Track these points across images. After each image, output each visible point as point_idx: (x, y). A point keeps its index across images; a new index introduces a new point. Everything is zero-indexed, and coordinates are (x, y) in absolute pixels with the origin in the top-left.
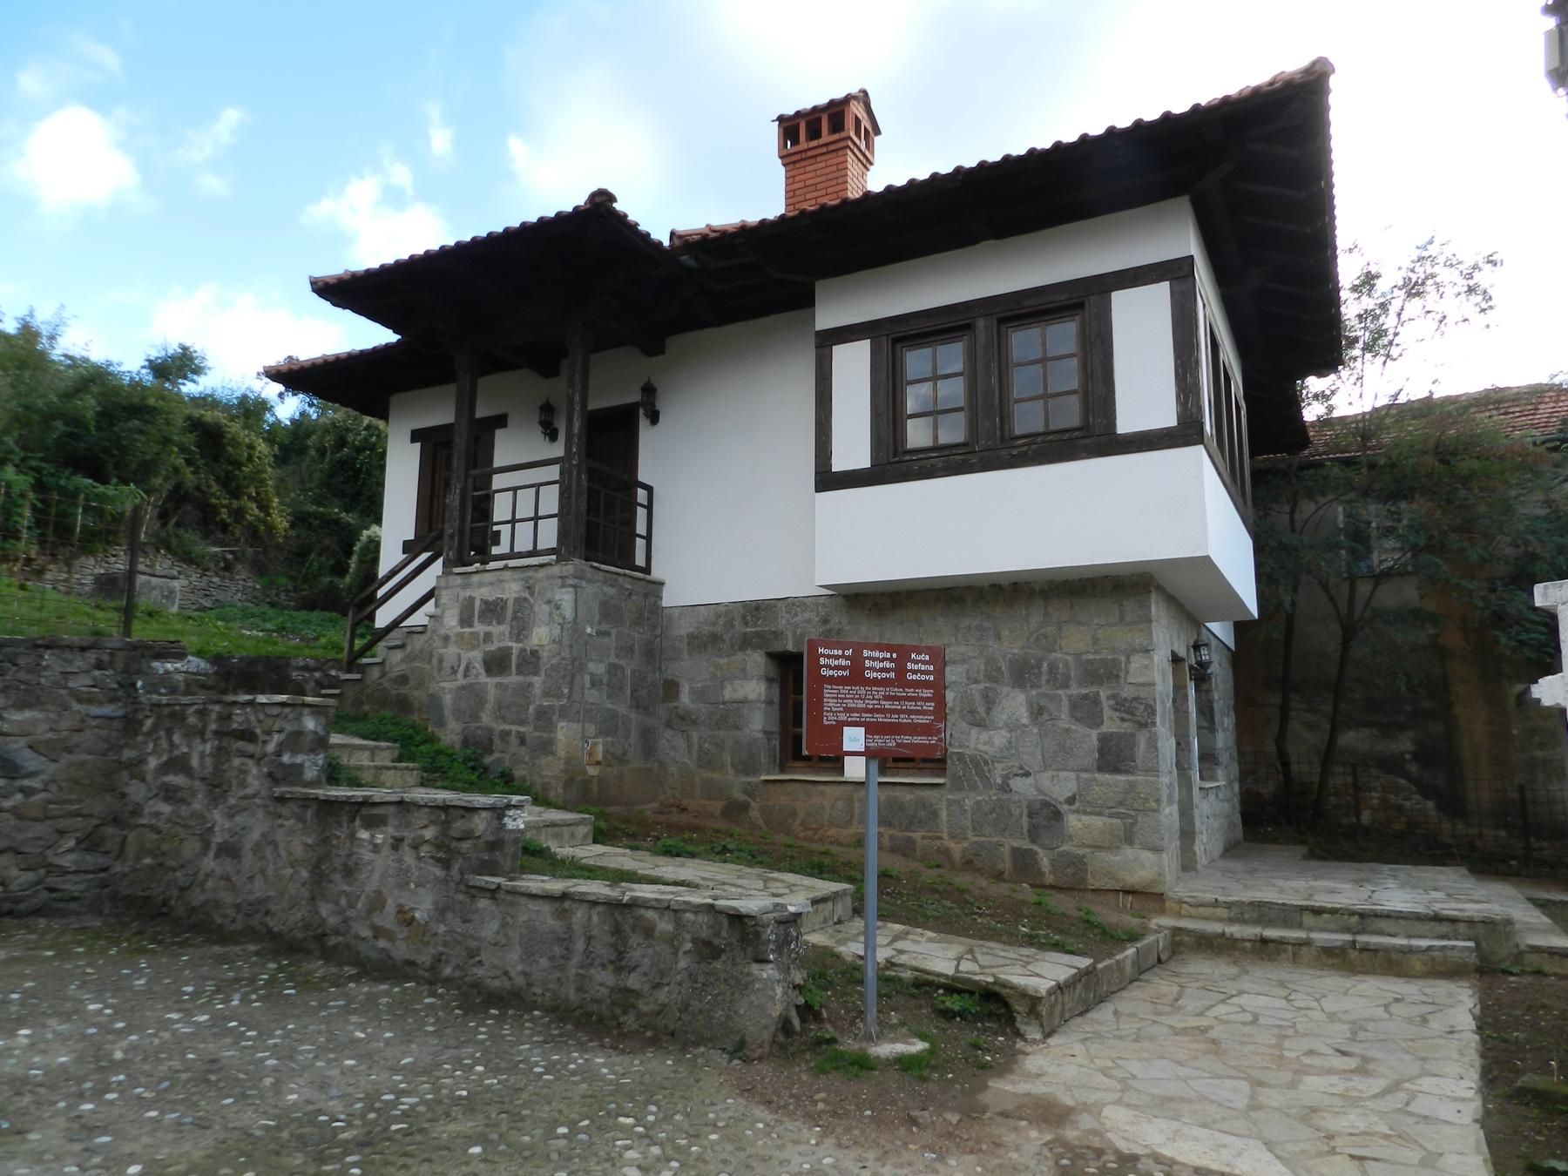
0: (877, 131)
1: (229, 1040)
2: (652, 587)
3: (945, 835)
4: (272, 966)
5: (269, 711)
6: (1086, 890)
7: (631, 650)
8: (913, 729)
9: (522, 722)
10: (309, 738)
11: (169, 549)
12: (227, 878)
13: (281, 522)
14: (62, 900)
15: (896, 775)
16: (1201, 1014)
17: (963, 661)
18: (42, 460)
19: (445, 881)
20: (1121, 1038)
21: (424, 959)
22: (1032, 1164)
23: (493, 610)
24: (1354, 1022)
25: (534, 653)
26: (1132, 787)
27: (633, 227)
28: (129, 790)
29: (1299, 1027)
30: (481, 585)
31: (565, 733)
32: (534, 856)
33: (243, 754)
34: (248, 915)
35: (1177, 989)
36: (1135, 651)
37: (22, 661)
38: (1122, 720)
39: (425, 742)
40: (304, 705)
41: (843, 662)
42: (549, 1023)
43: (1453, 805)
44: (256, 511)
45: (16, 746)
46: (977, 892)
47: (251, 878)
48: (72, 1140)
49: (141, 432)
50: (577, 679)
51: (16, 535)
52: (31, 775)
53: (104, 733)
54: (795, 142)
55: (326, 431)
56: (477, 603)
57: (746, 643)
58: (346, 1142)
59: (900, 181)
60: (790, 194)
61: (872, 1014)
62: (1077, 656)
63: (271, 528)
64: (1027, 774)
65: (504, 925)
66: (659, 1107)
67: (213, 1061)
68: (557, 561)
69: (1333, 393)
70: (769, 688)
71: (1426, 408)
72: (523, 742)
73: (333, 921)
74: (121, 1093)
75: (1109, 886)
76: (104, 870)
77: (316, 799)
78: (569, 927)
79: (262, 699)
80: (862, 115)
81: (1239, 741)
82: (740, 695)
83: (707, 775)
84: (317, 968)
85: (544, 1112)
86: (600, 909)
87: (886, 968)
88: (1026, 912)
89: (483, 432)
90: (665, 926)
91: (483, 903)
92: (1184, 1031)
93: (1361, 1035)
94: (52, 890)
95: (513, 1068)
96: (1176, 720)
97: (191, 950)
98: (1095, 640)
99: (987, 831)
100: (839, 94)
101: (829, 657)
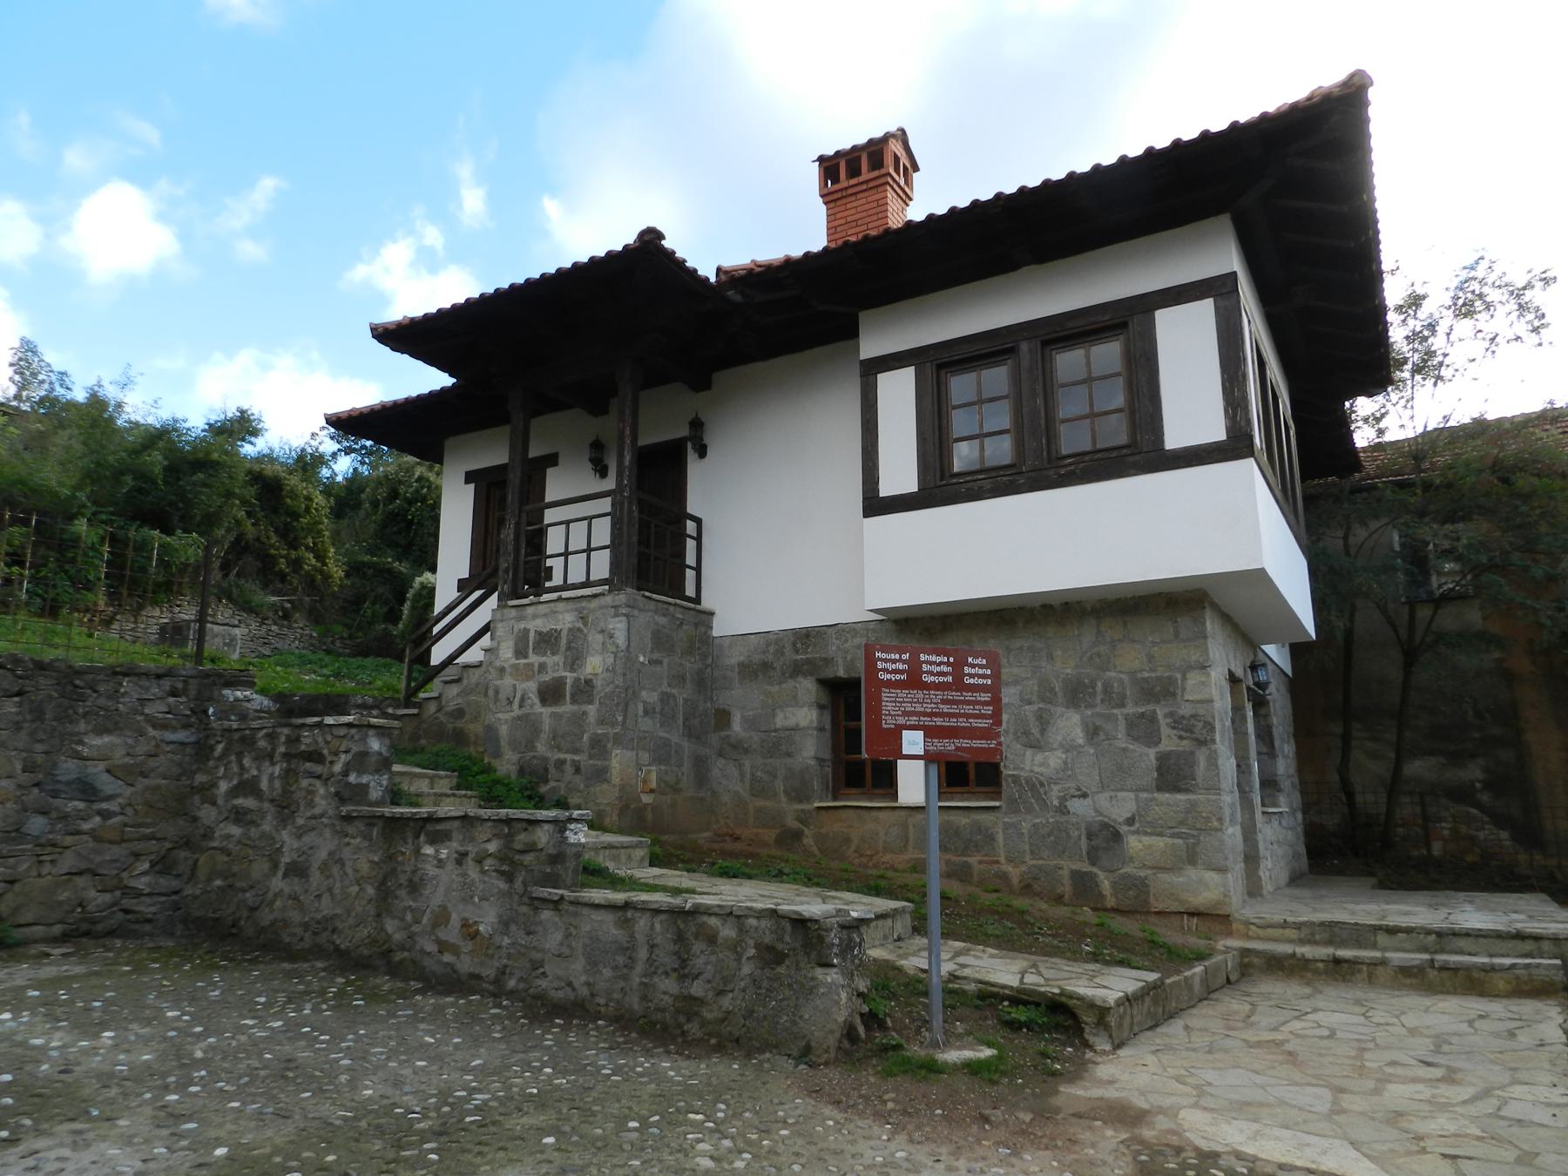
0: (916, 168)
1: (303, 1043)
2: (703, 617)
3: (1002, 860)
4: (341, 980)
5: (336, 732)
6: (1148, 913)
7: (683, 679)
8: (972, 733)
9: (576, 751)
10: (374, 759)
11: (230, 599)
12: (296, 898)
13: (337, 572)
14: (137, 922)
15: (952, 800)
16: (1275, 1029)
17: (1016, 683)
18: (112, 514)
19: (508, 894)
20: (1194, 1050)
21: (489, 972)
22: (1110, 1159)
23: (547, 641)
24: (1437, 1036)
25: (588, 682)
26: (1193, 805)
27: (681, 263)
28: (201, 814)
29: (1378, 1041)
30: (535, 617)
31: (619, 761)
32: (595, 874)
33: (311, 775)
34: (315, 934)
35: (1247, 1007)
36: (1191, 668)
37: (102, 689)
38: (1181, 738)
39: (482, 772)
40: (370, 726)
41: (901, 666)
42: (614, 1032)
43: (1530, 835)
44: (313, 561)
45: (95, 770)
46: (1037, 914)
47: (319, 897)
48: (158, 1126)
49: (205, 485)
50: (631, 707)
51: (89, 586)
52: (109, 798)
53: (178, 758)
54: (836, 181)
55: (379, 483)
56: (532, 635)
57: (797, 670)
58: (423, 1131)
59: (941, 210)
60: (832, 230)
61: (937, 1021)
62: (1132, 674)
63: (327, 577)
64: (1085, 796)
65: (568, 936)
66: (728, 1105)
67: (289, 1061)
68: (610, 591)
69: (1383, 416)
70: (821, 715)
71: (1479, 428)
72: (578, 770)
73: (398, 937)
74: (203, 1086)
75: (1173, 909)
76: (176, 893)
77: (382, 816)
78: (632, 936)
79: (329, 720)
80: (900, 152)
81: (1300, 770)
82: (791, 722)
83: (760, 803)
84: (385, 983)
85: (614, 1108)
86: (663, 917)
87: (950, 981)
88: (1088, 930)
89: (535, 471)
90: (728, 932)
91: (546, 915)
92: (1259, 1044)
93: (1446, 1048)
94: (126, 911)
95: (582, 1070)
96: (1236, 741)
97: (262, 966)
98: (1151, 658)
99: (1046, 853)
100: (878, 133)
101: (886, 661)
